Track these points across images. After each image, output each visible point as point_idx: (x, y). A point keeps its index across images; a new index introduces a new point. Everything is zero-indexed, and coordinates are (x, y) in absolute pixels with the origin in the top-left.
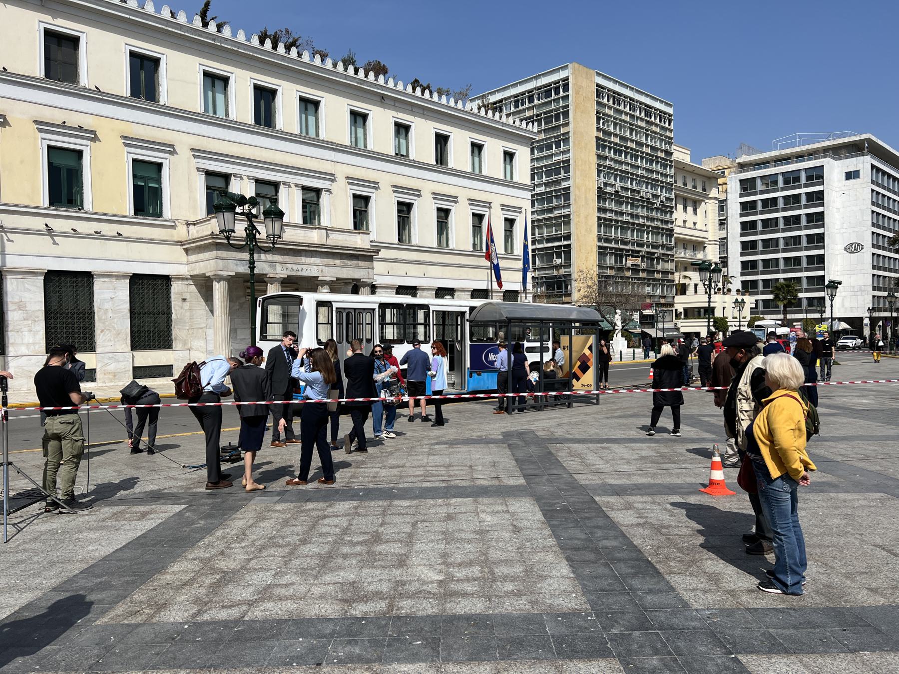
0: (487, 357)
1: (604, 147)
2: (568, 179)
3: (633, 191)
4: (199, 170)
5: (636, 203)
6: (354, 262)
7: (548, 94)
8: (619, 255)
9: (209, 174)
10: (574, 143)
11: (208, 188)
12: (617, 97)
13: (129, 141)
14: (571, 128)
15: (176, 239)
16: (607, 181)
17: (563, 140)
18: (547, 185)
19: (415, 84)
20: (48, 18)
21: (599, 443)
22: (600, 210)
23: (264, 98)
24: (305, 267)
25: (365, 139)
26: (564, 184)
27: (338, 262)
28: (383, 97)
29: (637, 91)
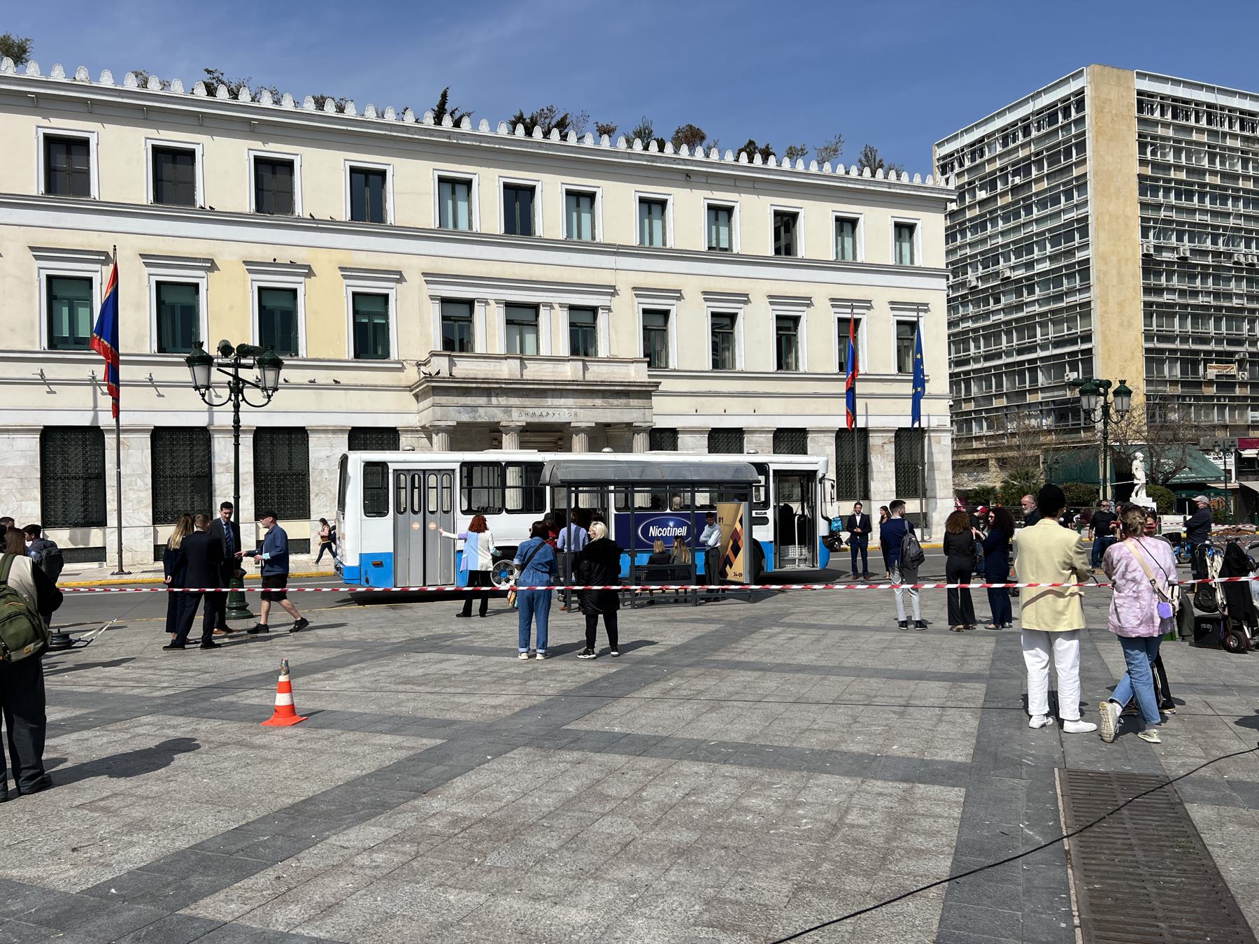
0: (645, 531)
1: (1155, 191)
2: (1085, 246)
3: (1217, 254)
4: (432, 298)
5: (1225, 274)
6: (623, 401)
7: (1052, 118)
8: (1190, 361)
9: (445, 301)
10: (1095, 189)
11: (444, 318)
12: (1179, 107)
13: (348, 272)
14: (1089, 167)
15: (404, 383)
16: (1162, 242)
17: (1078, 187)
18: (1052, 258)
19: (750, 149)
20: (258, 145)
21: (741, 662)
22: (1147, 290)
23: (519, 202)
24: (551, 411)
25: (664, 234)
26: (1080, 256)
27: (598, 402)
28: (688, 174)
29: (1221, 91)
